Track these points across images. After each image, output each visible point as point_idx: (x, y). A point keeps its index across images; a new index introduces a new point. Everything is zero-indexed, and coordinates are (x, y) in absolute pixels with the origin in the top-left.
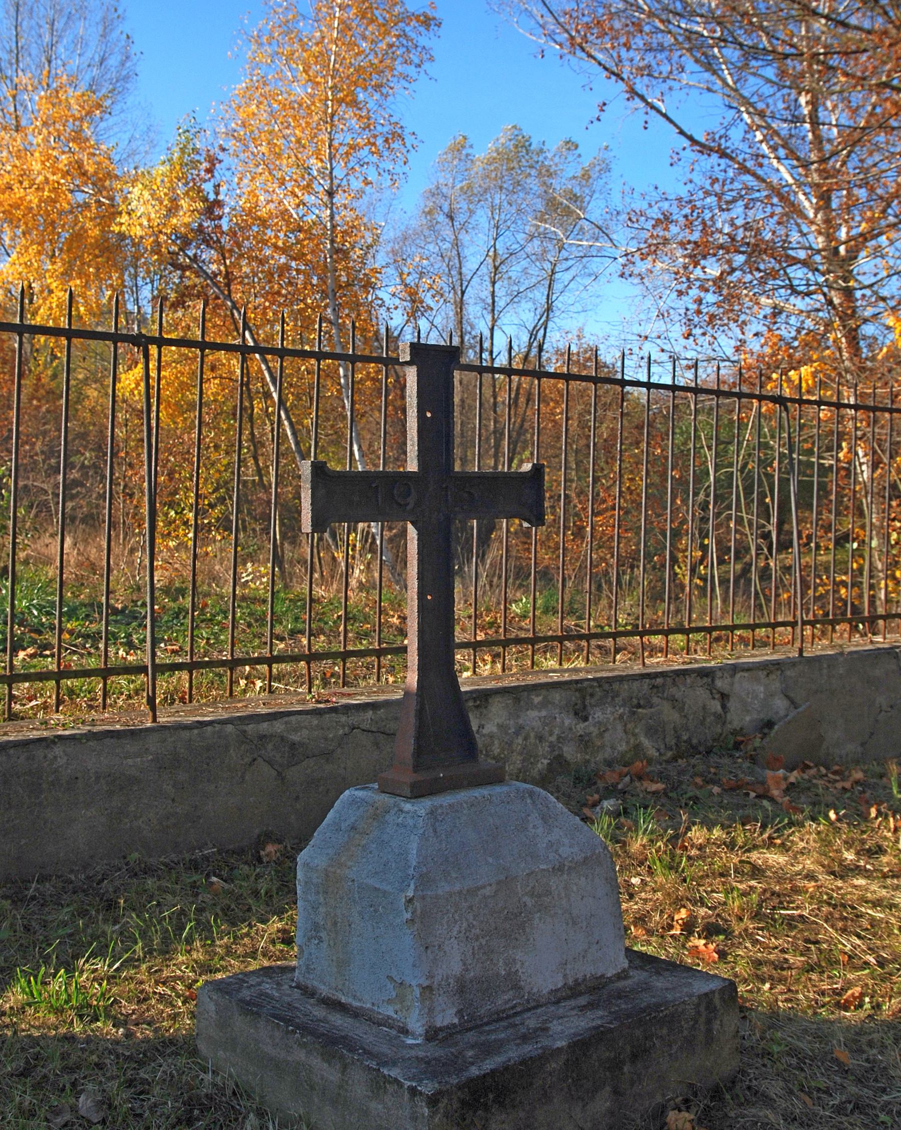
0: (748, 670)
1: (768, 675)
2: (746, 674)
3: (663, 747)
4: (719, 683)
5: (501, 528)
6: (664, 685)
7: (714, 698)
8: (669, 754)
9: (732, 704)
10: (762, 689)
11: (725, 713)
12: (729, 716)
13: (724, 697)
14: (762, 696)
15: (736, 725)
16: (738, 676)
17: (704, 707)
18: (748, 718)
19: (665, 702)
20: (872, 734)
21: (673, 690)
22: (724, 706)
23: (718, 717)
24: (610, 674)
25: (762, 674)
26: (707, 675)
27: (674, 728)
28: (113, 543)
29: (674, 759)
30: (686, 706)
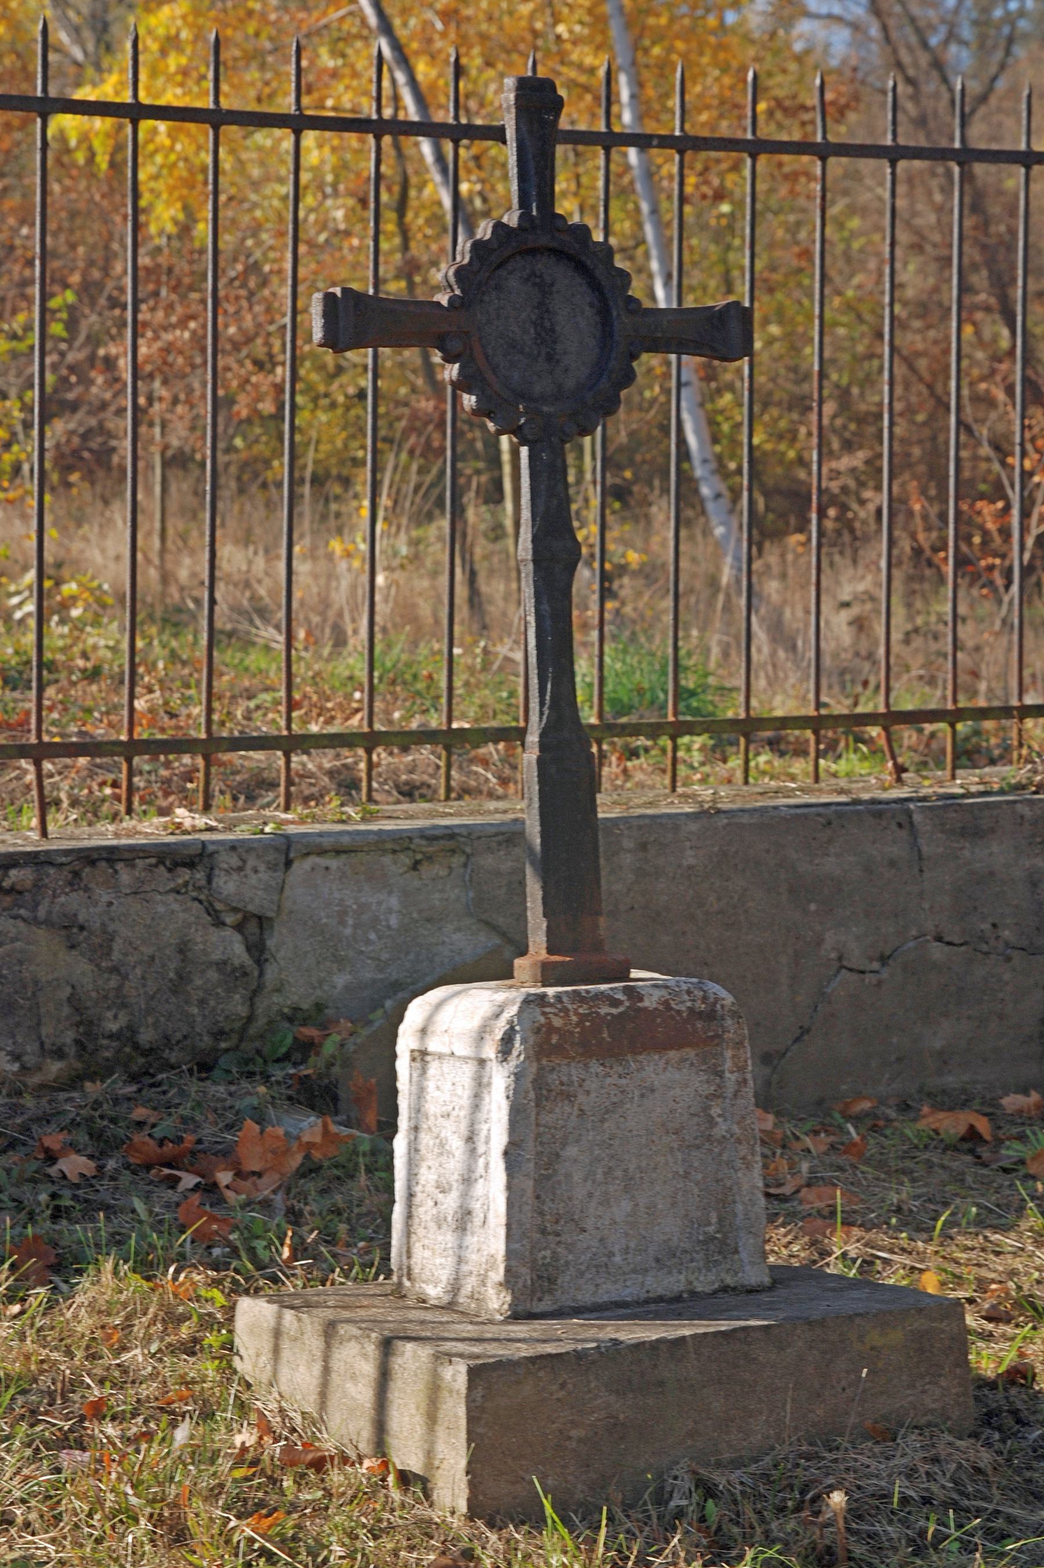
0: (338, 852)
1: (415, 866)
2: (333, 863)
3: (32, 1048)
4: (227, 885)
5: (123, 51)
6: (38, 886)
7: (219, 924)
8: (55, 1068)
9: (280, 941)
10: (394, 902)
11: (260, 963)
12: (271, 973)
13: (255, 926)
14: (394, 921)
15: (298, 994)
16: (301, 867)
17: (183, 949)
18: (341, 980)
19: (41, 933)
20: (805, 1031)
21: (72, 901)
22: (258, 950)
23: (233, 975)
24: (395, 1241)
25: (394, 866)
26: (190, 864)
27: (73, 1000)
28: (219, 533)
29: (74, 1082)
30: (117, 946)
